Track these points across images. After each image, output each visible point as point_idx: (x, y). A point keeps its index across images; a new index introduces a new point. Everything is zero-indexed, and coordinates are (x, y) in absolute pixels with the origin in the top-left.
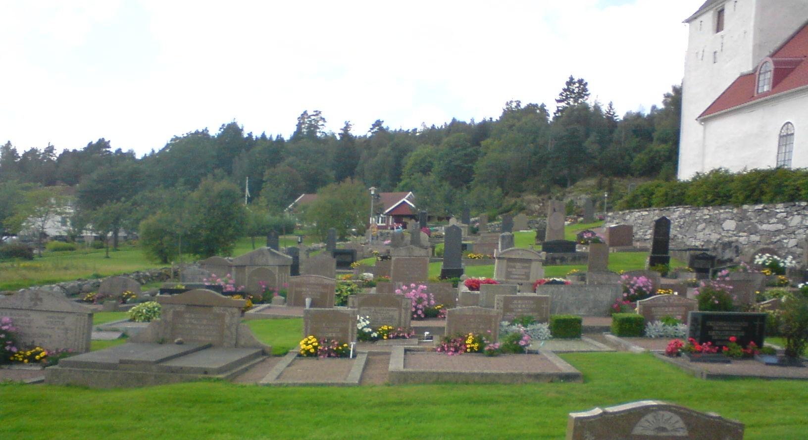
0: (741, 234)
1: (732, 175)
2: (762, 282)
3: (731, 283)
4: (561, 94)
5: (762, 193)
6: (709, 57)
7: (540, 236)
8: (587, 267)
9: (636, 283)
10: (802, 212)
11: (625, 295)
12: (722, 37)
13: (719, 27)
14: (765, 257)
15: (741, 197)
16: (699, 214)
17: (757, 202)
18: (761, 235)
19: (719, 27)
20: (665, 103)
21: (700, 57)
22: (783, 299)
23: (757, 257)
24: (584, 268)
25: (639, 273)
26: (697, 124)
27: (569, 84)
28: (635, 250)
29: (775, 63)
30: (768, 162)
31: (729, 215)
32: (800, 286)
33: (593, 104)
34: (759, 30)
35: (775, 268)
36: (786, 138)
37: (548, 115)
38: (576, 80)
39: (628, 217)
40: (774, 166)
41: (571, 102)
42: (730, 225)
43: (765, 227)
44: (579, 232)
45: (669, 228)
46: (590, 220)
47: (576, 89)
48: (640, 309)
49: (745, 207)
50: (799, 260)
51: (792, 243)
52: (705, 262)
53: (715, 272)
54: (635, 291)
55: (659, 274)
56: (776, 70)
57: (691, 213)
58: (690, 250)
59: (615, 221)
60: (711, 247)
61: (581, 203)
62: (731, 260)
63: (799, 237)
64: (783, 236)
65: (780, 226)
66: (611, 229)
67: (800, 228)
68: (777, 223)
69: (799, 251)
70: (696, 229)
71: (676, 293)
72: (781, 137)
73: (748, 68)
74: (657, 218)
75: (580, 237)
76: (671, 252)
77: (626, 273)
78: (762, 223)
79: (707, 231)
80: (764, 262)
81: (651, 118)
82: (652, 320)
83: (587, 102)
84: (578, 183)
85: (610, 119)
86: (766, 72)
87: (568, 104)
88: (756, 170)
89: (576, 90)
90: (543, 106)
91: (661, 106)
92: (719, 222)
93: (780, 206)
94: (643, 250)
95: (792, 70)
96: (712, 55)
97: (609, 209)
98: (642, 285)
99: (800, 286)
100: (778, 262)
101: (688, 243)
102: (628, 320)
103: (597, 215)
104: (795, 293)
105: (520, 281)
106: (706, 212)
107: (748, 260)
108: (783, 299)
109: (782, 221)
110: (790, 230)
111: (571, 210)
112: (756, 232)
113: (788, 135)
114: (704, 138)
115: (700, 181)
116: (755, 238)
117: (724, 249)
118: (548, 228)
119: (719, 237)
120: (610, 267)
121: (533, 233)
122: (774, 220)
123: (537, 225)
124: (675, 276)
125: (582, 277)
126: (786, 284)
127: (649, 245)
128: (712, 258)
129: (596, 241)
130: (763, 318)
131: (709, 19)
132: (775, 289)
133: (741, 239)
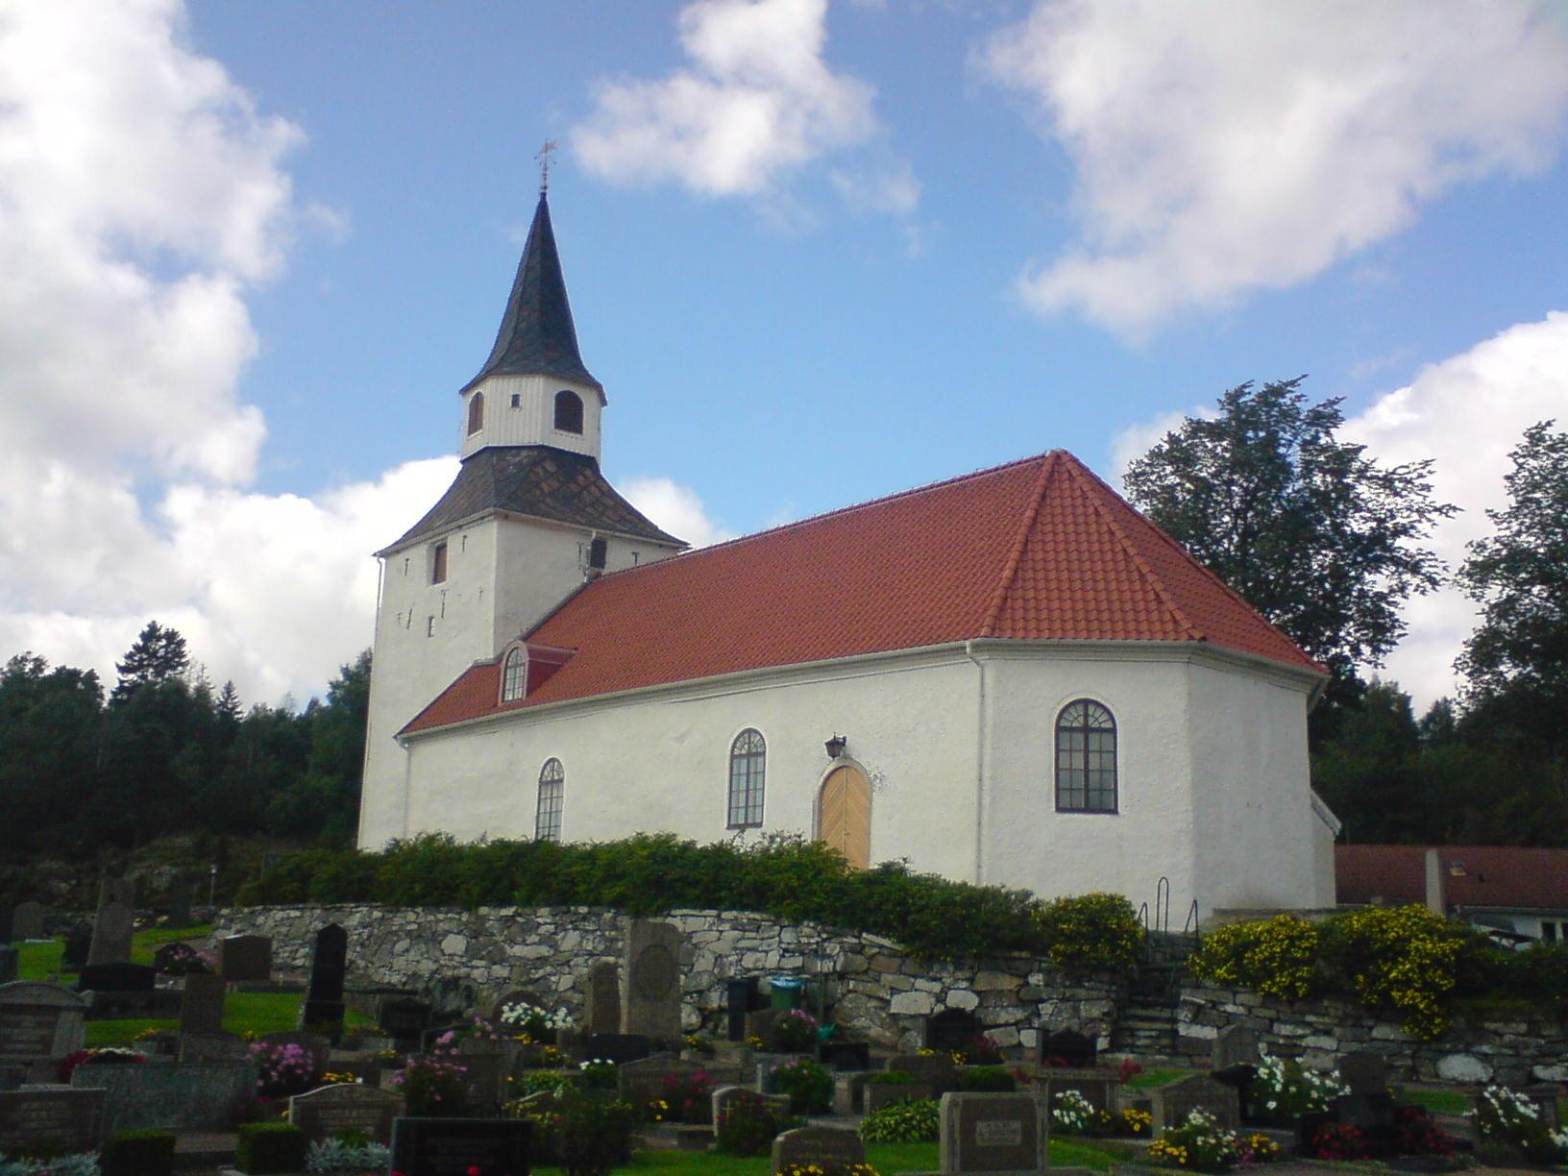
0: (475, 963)
1: (461, 848)
2: (518, 1057)
3: (461, 1059)
4: (130, 656)
5: (514, 886)
6: (419, 625)
7: (75, 953)
8: (175, 1022)
9: (282, 1057)
10: (581, 925)
11: (261, 1083)
12: (443, 592)
13: (438, 575)
14: (519, 1010)
15: (476, 890)
16: (398, 920)
17: (504, 903)
19: (438, 575)
20: (331, 696)
22: (558, 1093)
23: (506, 1008)
24: (172, 1025)
25: (284, 1038)
26: (396, 744)
27: (145, 636)
28: (275, 988)
29: (532, 653)
30: (521, 830)
31: (453, 926)
32: (584, 1065)
33: (193, 685)
34: (504, 592)
35: (536, 1027)
36: (550, 782)
37: (102, 696)
38: (162, 632)
39: (260, 920)
40: (532, 837)
41: (150, 673)
42: (455, 944)
43: (518, 950)
44: (158, 947)
45: (344, 948)
46: (181, 921)
47: (159, 650)
48: (295, 1113)
49: (484, 910)
50: (578, 1015)
51: (565, 982)
52: (411, 1015)
53: (431, 1039)
54: (281, 1075)
55: (327, 1041)
58: (380, 991)
59: (235, 927)
60: (420, 986)
61: (161, 883)
62: (457, 1014)
65: (544, 950)
66: (228, 944)
68: (540, 943)
69: (577, 998)
70: (401, 951)
71: (360, 1080)
72: (542, 783)
73: (487, 654)
74: (320, 926)
75: (163, 956)
76: (345, 995)
77: (263, 1039)
78: (512, 942)
79: (412, 955)
80: (518, 1019)
81: (305, 722)
82: (320, 1134)
83: (184, 677)
84: (157, 842)
85: (228, 714)
86: (516, 666)
87: (144, 677)
88: (501, 841)
89: (162, 652)
90: (91, 676)
91: (325, 703)
92: (435, 939)
93: (544, 911)
94: (290, 988)
95: (556, 669)
97: (223, 900)
98: (292, 1061)
99: (584, 1065)
100: (543, 1019)
102: (271, 1136)
103: (195, 912)
104: (576, 1080)
105: (28, 1057)
106: (411, 916)
107: (489, 1014)
108: (558, 1093)
109: (548, 940)
110: (562, 958)
111: (144, 899)
113: (553, 781)
114: (408, 773)
115: (399, 855)
116: (500, 971)
117: (445, 992)
118: (94, 936)
119: (434, 967)
120: (229, 1024)
121: (54, 946)
122: (534, 938)
123: (68, 929)
124: (354, 1045)
125: (167, 1045)
126: (559, 1064)
127: (304, 980)
128: (424, 1010)
129: (196, 968)
130: (527, 1127)
131: (420, 557)
132: (541, 1073)
133: (476, 973)
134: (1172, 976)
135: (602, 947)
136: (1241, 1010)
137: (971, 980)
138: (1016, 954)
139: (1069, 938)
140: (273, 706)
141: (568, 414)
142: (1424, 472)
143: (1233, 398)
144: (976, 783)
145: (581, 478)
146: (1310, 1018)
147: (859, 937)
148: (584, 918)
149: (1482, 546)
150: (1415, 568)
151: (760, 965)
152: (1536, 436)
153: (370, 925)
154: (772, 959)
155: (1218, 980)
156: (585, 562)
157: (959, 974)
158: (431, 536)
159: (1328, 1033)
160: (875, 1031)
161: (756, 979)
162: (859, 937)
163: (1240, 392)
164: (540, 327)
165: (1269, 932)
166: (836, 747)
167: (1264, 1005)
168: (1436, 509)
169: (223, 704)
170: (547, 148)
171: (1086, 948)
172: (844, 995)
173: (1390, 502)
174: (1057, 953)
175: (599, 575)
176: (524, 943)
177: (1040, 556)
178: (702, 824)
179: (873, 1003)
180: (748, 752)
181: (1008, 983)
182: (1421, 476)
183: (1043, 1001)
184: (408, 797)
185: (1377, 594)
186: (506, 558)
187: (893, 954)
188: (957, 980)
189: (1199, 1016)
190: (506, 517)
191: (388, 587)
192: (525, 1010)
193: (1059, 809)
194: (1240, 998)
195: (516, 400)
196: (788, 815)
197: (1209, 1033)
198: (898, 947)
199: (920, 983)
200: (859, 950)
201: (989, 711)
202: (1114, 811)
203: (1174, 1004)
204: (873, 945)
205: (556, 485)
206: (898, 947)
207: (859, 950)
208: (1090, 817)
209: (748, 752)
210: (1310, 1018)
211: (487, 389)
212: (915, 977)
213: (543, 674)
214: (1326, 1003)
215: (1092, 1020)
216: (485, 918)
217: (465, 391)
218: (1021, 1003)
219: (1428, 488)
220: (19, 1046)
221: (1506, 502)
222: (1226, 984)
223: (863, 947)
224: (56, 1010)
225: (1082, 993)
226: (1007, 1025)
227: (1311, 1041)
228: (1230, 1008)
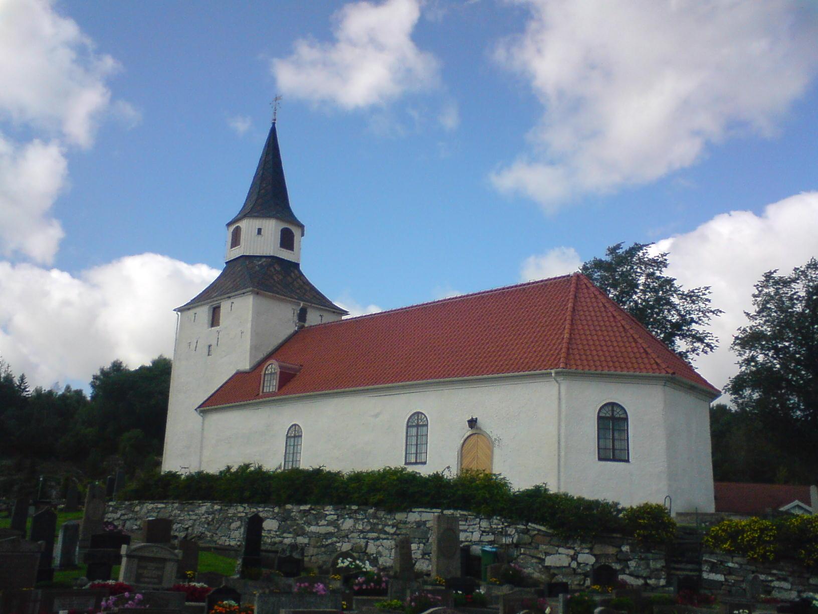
0: (285, 535)
12: (218, 332)
13: (214, 321)
16: (231, 511)
17: (300, 503)
18: (310, 538)
19: (214, 321)
21: (193, 346)
30: (396, 461)
34: (255, 333)
36: (294, 435)
39: (137, 508)
43: (313, 529)
49: (289, 506)
56: (281, 373)
57: (221, 509)
63: (353, 541)
64: (335, 539)
65: (331, 529)
67: (353, 532)
68: (328, 525)
78: (310, 524)
95: (294, 376)
96: (207, 348)
101: (220, 542)
106: (240, 509)
110: (343, 533)
112: (304, 534)
122: (323, 522)
131: (204, 313)
135: (369, 528)
136: (736, 566)
137: (591, 549)
138: (615, 535)
139: (644, 527)
140: (46, 388)
141: (287, 240)
142: (706, 292)
143: (613, 251)
144: (557, 445)
145: (293, 275)
146: (775, 572)
147: (526, 525)
148: (356, 512)
149: (745, 330)
150: (701, 340)
152: (768, 276)
153: (213, 513)
154: (476, 536)
155: (725, 549)
156: (296, 319)
157: (584, 546)
158: (211, 299)
159: (785, 580)
160: (536, 575)
161: (468, 547)
162: (526, 525)
163: (618, 247)
164: (269, 193)
165: (750, 525)
166: (472, 423)
167: (748, 563)
168: (711, 311)
169: (19, 386)
170: (276, 99)
171: (653, 532)
172: (518, 556)
173: (689, 307)
174: (639, 535)
175: (303, 326)
176: (317, 524)
177: (580, 327)
178: (272, 461)
179: (534, 560)
180: (417, 424)
181: (611, 550)
182: (704, 294)
183: (630, 560)
184: (196, 444)
185: (680, 353)
186: (257, 314)
187: (546, 534)
188: (583, 548)
189: (714, 568)
190: (258, 293)
191: (181, 328)
192: (351, 563)
193: (600, 459)
194: (736, 559)
195: (259, 231)
196: (441, 460)
197: (720, 578)
198: (550, 531)
199: (561, 550)
200: (526, 532)
201: (563, 406)
202: (627, 461)
203: (700, 563)
204: (535, 529)
205: (281, 277)
206: (550, 531)
207: (526, 532)
208: (616, 463)
209: (417, 424)
210: (775, 572)
211: (244, 224)
212: (559, 546)
213: (286, 378)
214: (782, 564)
215: (657, 570)
216: (290, 511)
217: (229, 225)
219: (709, 301)
220: (146, 580)
221: (753, 310)
222: (729, 552)
223: (528, 530)
224: (164, 560)
225: (650, 555)
227: (776, 584)
228: (730, 565)
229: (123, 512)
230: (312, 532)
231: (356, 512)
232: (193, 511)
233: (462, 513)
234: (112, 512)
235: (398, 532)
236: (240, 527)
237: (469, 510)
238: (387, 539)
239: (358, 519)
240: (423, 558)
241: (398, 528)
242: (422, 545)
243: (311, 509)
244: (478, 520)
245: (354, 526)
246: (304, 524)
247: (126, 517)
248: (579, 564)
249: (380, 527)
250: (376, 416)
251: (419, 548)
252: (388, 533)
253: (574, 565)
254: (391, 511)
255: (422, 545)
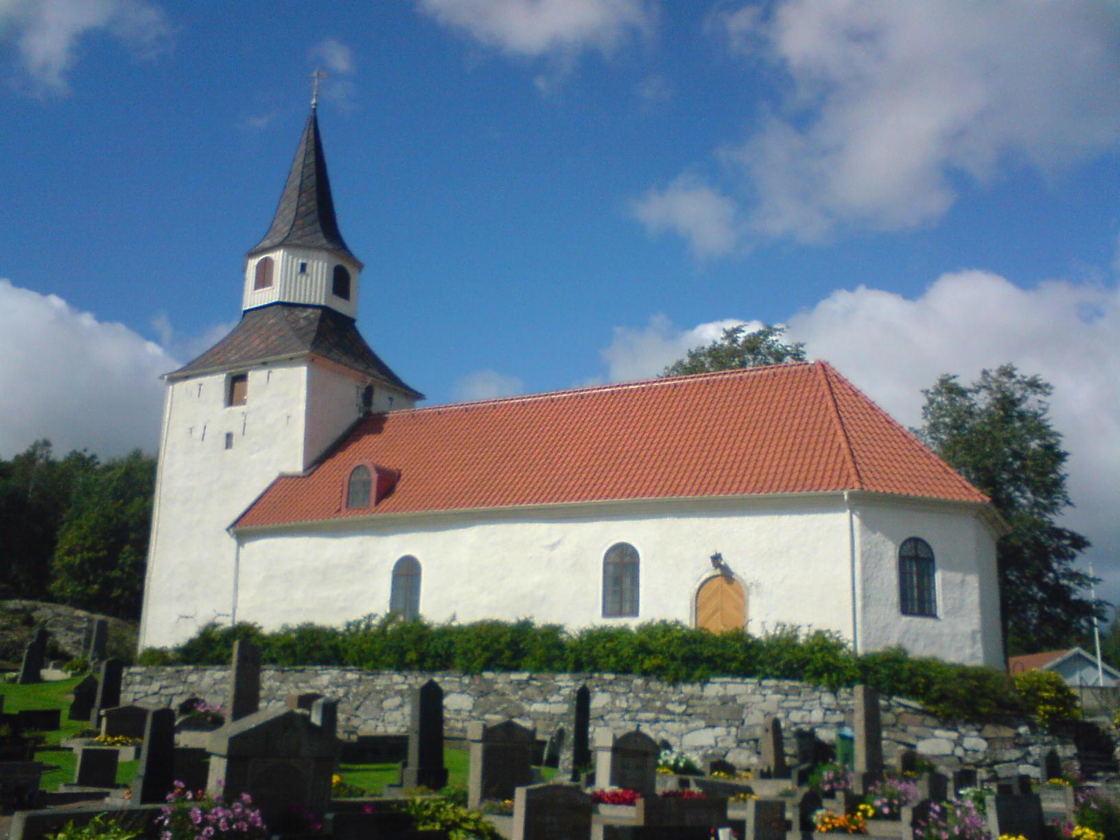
13: (234, 393)
16: (381, 682)
17: (509, 669)
18: (535, 720)
19: (234, 393)
21: (198, 433)
36: (407, 575)
43: (538, 707)
49: (488, 675)
57: (360, 680)
67: (611, 711)
78: (531, 700)
122: (555, 698)
131: (216, 383)
134: (31, 744)
141: (341, 283)
151: (807, 720)
154: (817, 716)
166: (716, 559)
176: (545, 700)
181: (1008, 732)
183: (1032, 744)
187: (917, 711)
195: (303, 267)
199: (938, 732)
202: (933, 615)
204: (900, 705)
212: (935, 728)
216: (492, 682)
218: (1017, 746)
226: (1010, 761)
229: (165, 683)
230: (536, 712)
231: (611, 683)
232: (307, 682)
233: (792, 683)
234: (141, 683)
235: (690, 711)
236: (401, 706)
237: (801, 679)
238: (673, 721)
239: (617, 694)
240: (738, 746)
241: (688, 706)
242: (733, 730)
243: (531, 678)
244: (817, 694)
245: (613, 702)
246: (522, 699)
247: (171, 691)
248: (966, 750)
249: (658, 704)
250: (553, 546)
251: (729, 733)
252: (673, 713)
253: (959, 752)
254: (675, 682)
255: (733, 730)
